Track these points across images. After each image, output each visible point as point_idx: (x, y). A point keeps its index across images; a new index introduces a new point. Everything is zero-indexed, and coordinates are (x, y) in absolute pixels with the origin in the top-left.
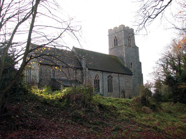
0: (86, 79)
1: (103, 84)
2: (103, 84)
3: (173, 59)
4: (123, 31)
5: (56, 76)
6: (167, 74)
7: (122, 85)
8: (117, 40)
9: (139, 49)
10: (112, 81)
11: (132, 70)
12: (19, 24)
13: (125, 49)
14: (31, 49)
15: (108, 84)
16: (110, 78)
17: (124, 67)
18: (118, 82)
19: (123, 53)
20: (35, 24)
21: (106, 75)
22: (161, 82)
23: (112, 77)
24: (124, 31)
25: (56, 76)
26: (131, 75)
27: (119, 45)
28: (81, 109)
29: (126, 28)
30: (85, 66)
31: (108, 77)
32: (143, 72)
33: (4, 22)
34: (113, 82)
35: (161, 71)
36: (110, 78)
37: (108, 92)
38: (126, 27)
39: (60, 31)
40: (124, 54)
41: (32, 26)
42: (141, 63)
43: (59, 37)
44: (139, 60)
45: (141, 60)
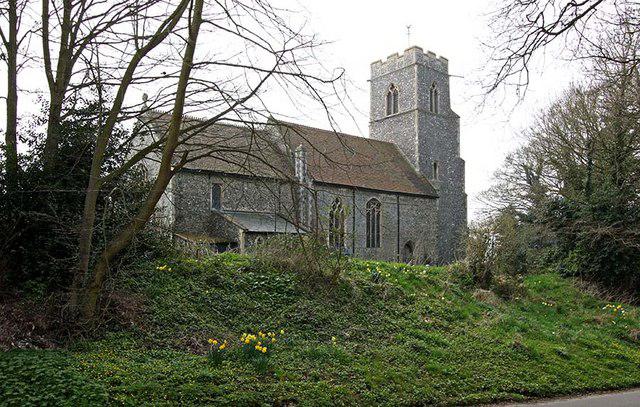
0: (307, 213)
1: (354, 227)
2: (354, 227)
3: (568, 147)
4: (416, 68)
5: (225, 204)
6: (537, 190)
7: (405, 227)
8: (395, 95)
9: (462, 122)
10: (378, 215)
11: (436, 183)
12: (141, 53)
13: (420, 122)
14: (175, 131)
15: (368, 223)
16: (217, 187)
17: (412, 176)
18: (396, 218)
19: (408, 135)
20: (198, 57)
21: (362, 201)
22: (517, 217)
23: (379, 205)
24: (419, 65)
25: (225, 204)
26: (434, 198)
27: (400, 111)
28: (313, 292)
29: (425, 58)
30: (304, 175)
31: (368, 205)
32: (468, 190)
33: (78, 48)
34: (381, 217)
35: (520, 184)
36: (217, 187)
37: (368, 246)
38: (425, 52)
39: (254, 79)
40: (417, 138)
41: (188, 65)
42: (463, 162)
43: (254, 93)
44: (458, 153)
45: (463, 154)
